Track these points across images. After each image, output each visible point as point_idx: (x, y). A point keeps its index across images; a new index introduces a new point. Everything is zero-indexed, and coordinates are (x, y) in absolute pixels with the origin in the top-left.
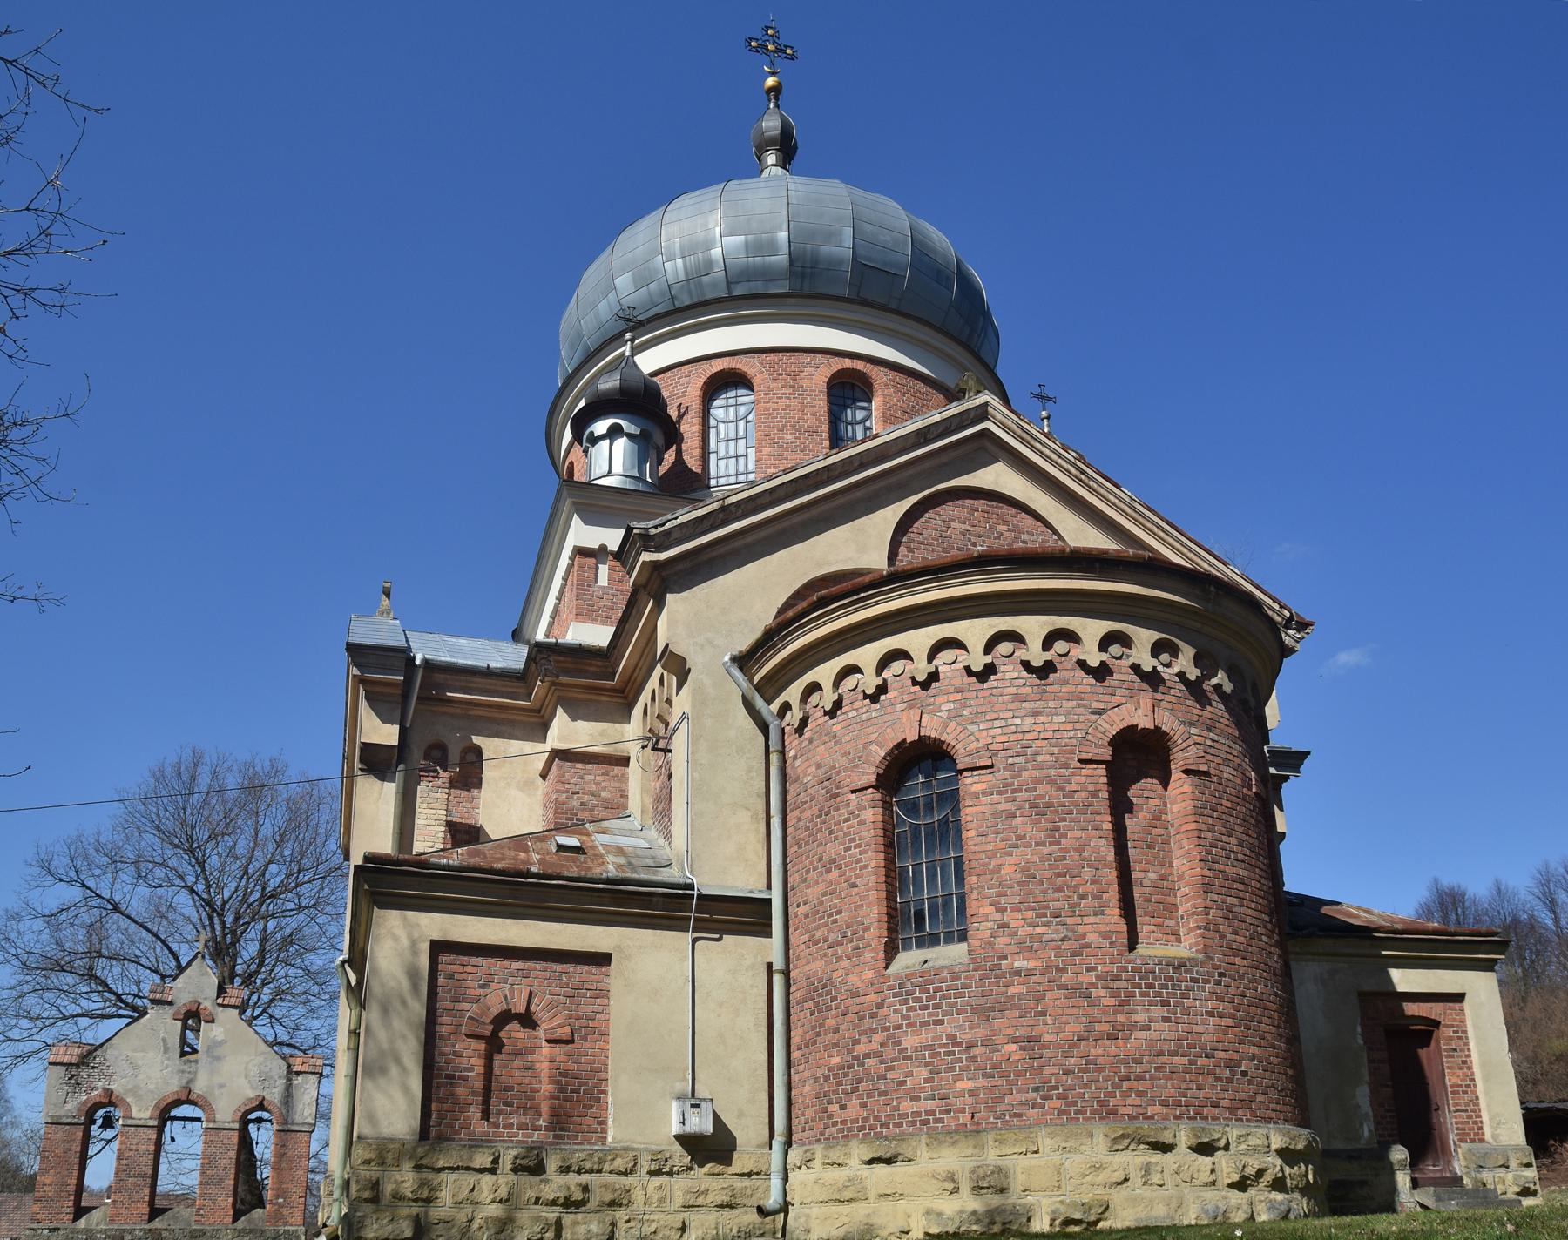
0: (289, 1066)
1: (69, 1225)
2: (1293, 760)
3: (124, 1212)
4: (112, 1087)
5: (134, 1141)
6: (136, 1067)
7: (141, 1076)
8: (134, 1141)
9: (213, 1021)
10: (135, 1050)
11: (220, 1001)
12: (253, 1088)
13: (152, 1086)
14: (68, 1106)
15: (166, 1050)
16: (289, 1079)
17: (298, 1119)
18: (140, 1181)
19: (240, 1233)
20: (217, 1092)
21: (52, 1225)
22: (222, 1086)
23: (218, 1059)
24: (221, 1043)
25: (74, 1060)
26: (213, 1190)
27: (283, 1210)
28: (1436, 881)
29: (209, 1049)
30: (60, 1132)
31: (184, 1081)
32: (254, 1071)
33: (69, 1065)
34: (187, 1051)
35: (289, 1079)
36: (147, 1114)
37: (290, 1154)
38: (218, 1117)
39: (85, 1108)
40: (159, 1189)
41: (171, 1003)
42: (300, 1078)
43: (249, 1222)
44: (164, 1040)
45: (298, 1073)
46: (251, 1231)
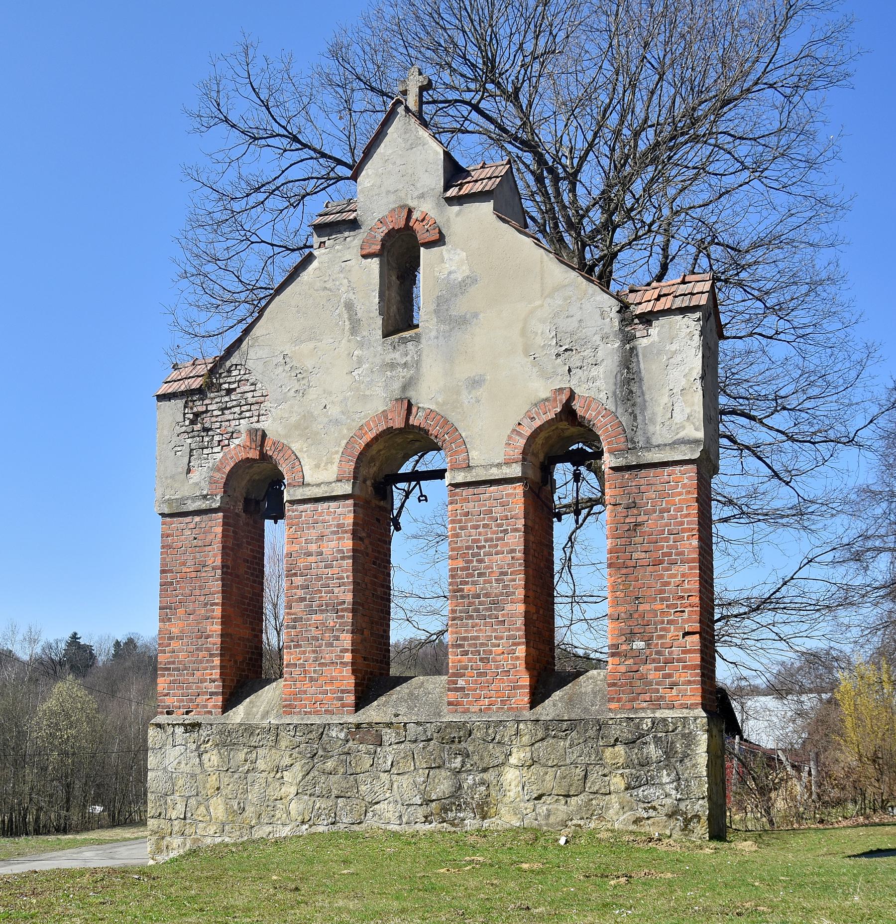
0: (624, 307)
1: (217, 717)
2: (276, 523)
3: (307, 686)
4: (265, 424)
5: (313, 534)
6: (299, 374)
7: (312, 394)
8: (313, 534)
9: (440, 241)
10: (297, 341)
11: (453, 192)
12: (545, 375)
13: (334, 411)
14: (195, 477)
15: (355, 326)
16: (628, 339)
17: (660, 433)
18: (331, 619)
19: (550, 730)
20: (466, 397)
21: (189, 719)
22: (475, 383)
23: (462, 322)
24: (464, 286)
25: (196, 384)
26: (482, 631)
27: (650, 671)
28: (74, 636)
29: (441, 304)
30: (186, 527)
31: (397, 385)
32: (542, 334)
33: (188, 393)
34: (399, 317)
35: (628, 339)
36: (330, 473)
37: (651, 524)
38: (476, 456)
39: (221, 477)
40: (399, 633)
41: (354, 225)
42: (654, 331)
43: (570, 702)
44: (349, 306)
45: (647, 319)
46: (573, 724)
